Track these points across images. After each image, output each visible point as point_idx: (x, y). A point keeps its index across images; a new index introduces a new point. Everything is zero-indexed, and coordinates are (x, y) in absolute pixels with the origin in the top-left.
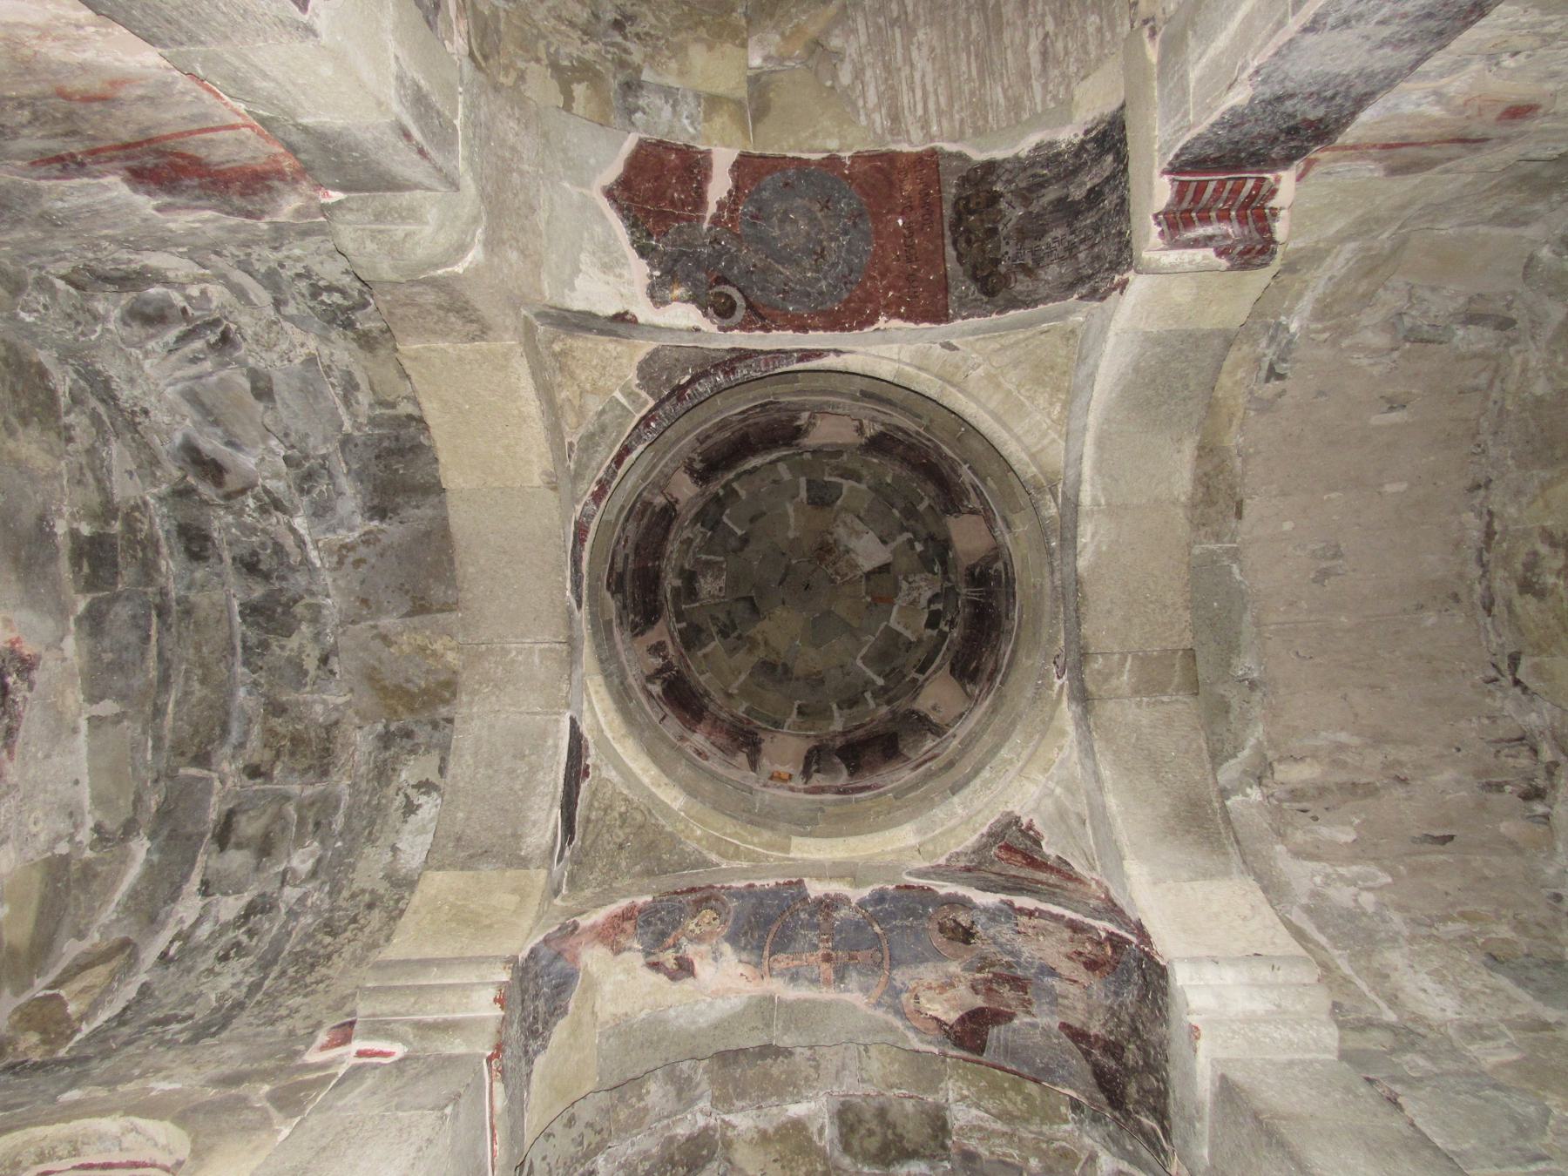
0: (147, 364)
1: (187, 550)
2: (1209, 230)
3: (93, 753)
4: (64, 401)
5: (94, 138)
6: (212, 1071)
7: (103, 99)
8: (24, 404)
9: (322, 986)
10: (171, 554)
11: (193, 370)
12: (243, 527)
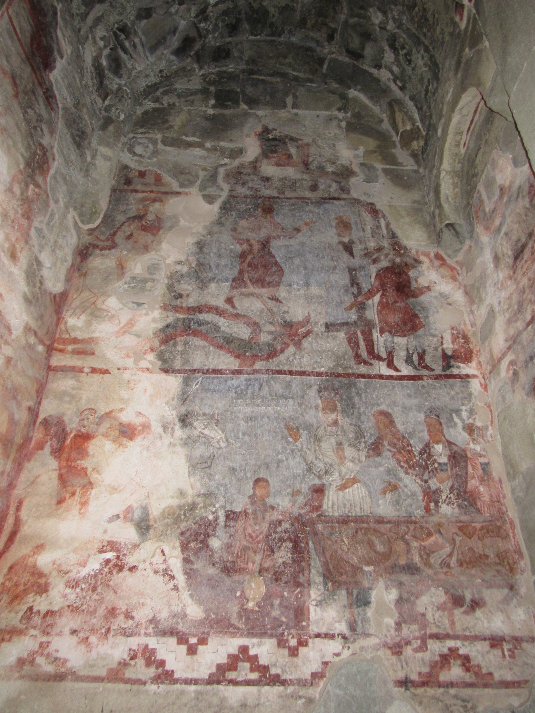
0: (139, 69)
1: (224, 58)
3: (308, 108)
4: (158, 105)
5: (33, 84)
6: (451, 74)
7: (13, 78)
8: (159, 121)
9: (436, 16)
10: (226, 66)
11: (139, 47)
12: (216, 28)
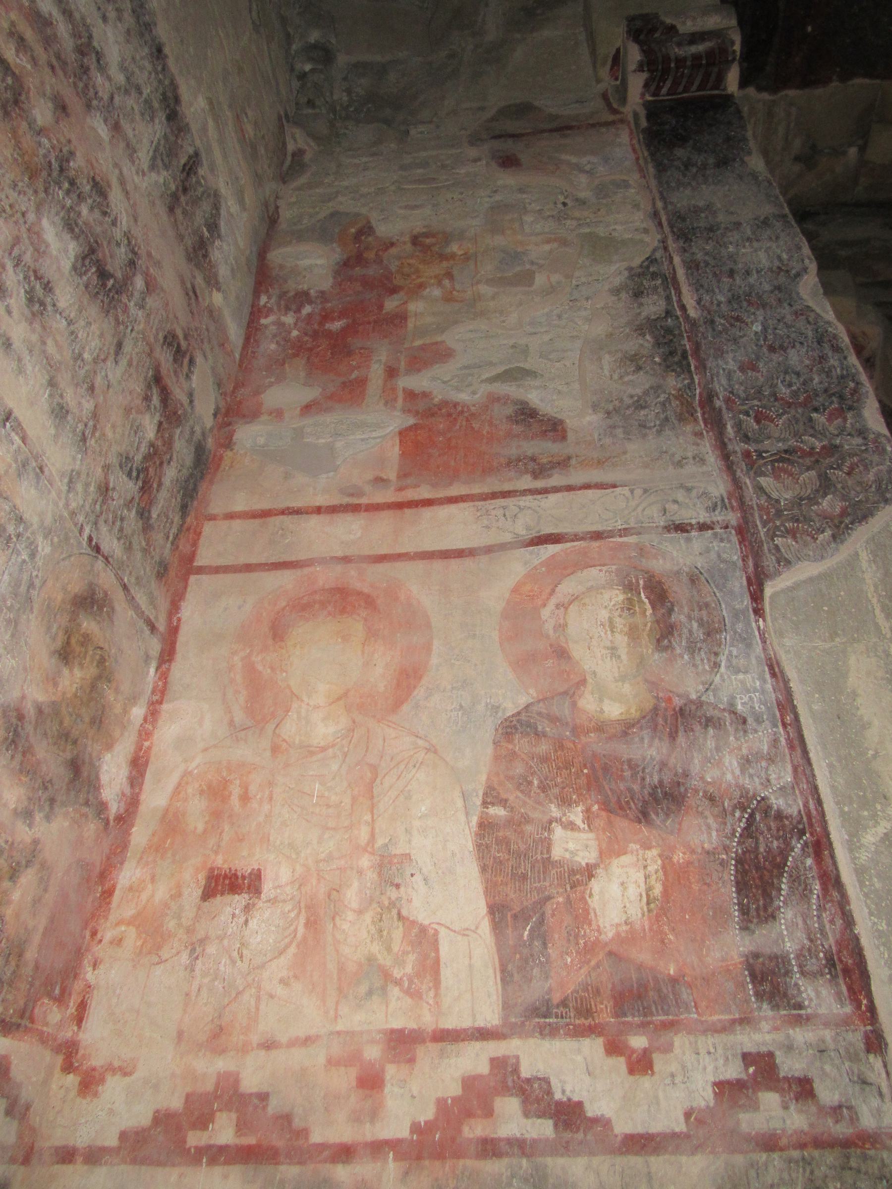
2: (694, 49)
